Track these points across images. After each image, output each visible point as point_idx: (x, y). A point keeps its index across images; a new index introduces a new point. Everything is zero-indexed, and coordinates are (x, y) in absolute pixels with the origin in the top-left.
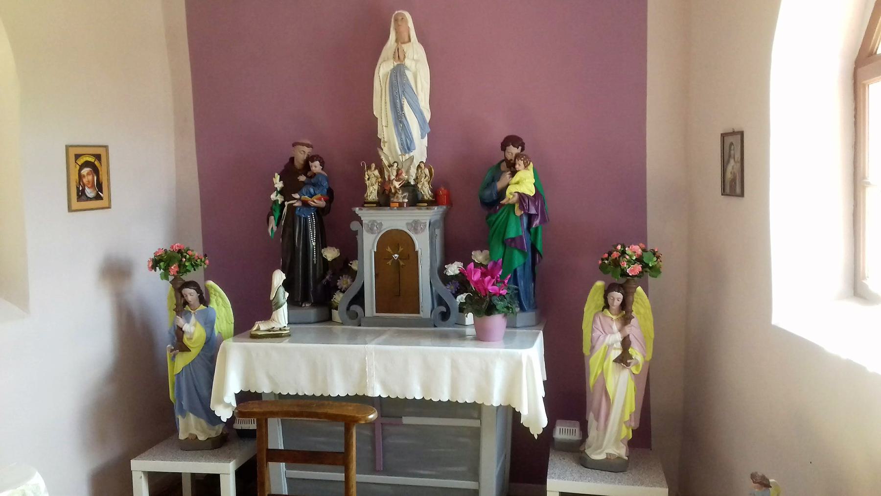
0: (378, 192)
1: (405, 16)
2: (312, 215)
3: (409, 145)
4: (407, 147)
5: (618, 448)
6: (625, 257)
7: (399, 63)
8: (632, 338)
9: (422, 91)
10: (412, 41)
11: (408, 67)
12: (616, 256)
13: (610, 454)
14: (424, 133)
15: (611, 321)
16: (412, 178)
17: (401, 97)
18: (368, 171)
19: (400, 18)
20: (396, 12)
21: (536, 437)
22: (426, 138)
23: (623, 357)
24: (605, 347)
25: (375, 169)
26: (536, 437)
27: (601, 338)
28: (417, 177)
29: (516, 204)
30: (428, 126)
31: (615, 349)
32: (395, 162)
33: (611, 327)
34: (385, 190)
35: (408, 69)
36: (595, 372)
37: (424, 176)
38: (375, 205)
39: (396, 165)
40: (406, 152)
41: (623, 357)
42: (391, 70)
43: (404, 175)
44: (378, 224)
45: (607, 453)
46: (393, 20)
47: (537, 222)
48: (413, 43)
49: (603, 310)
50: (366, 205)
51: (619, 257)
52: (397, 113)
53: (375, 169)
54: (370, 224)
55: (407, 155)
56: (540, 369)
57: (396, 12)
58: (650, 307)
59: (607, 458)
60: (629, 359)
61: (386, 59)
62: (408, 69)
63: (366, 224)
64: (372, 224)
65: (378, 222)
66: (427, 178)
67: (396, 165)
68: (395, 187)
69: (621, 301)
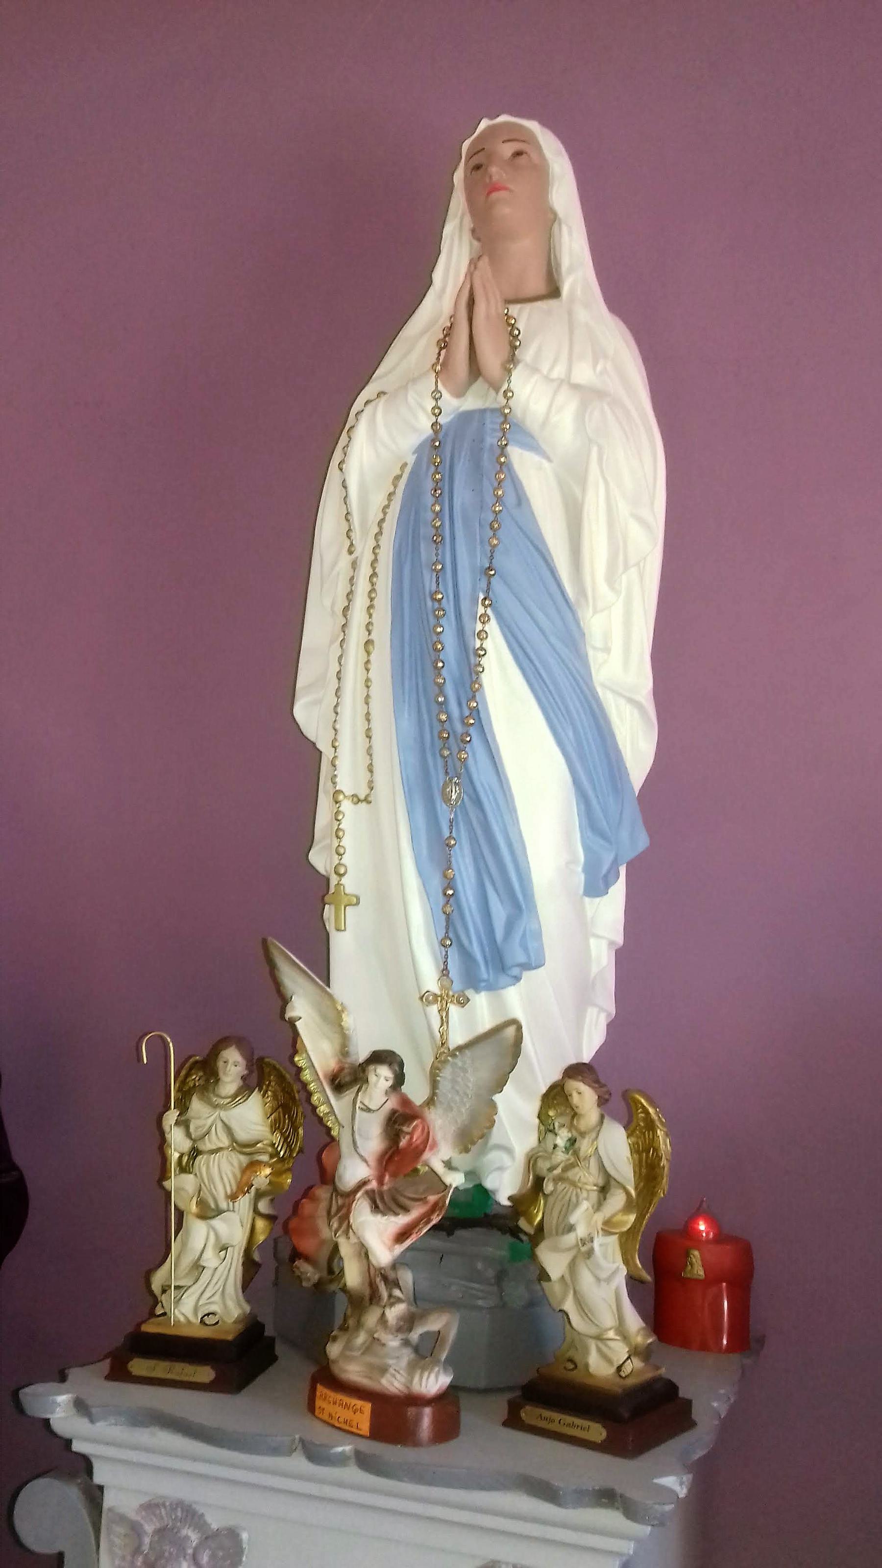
0: (250, 1266)
1: (529, 139)
3: (499, 934)
4: (277, 1134)
7: (471, 402)
9: (611, 580)
10: (565, 290)
11: (533, 424)
14: (607, 859)
16: (505, 1158)
17: (465, 605)
18: (196, 1105)
19: (507, 150)
20: (484, 124)
22: (618, 890)
25: (246, 1088)
28: (539, 1182)
30: (632, 812)
32: (378, 1057)
34: (296, 1255)
35: (531, 444)
37: (589, 1177)
38: (205, 1374)
39: (382, 1076)
40: (473, 982)
42: (419, 450)
43: (435, 1160)
44: (209, 1537)
46: (459, 176)
48: (572, 299)
50: (139, 1366)
53: (246, 1088)
54: (149, 1528)
55: (480, 1000)
56: (524, 835)
57: (484, 124)
61: (607, 1097)
62: (531, 444)
63: (122, 1519)
64: (161, 1532)
65: (215, 1522)
66: (617, 1200)
67: (382, 1076)
68: (364, 1253)
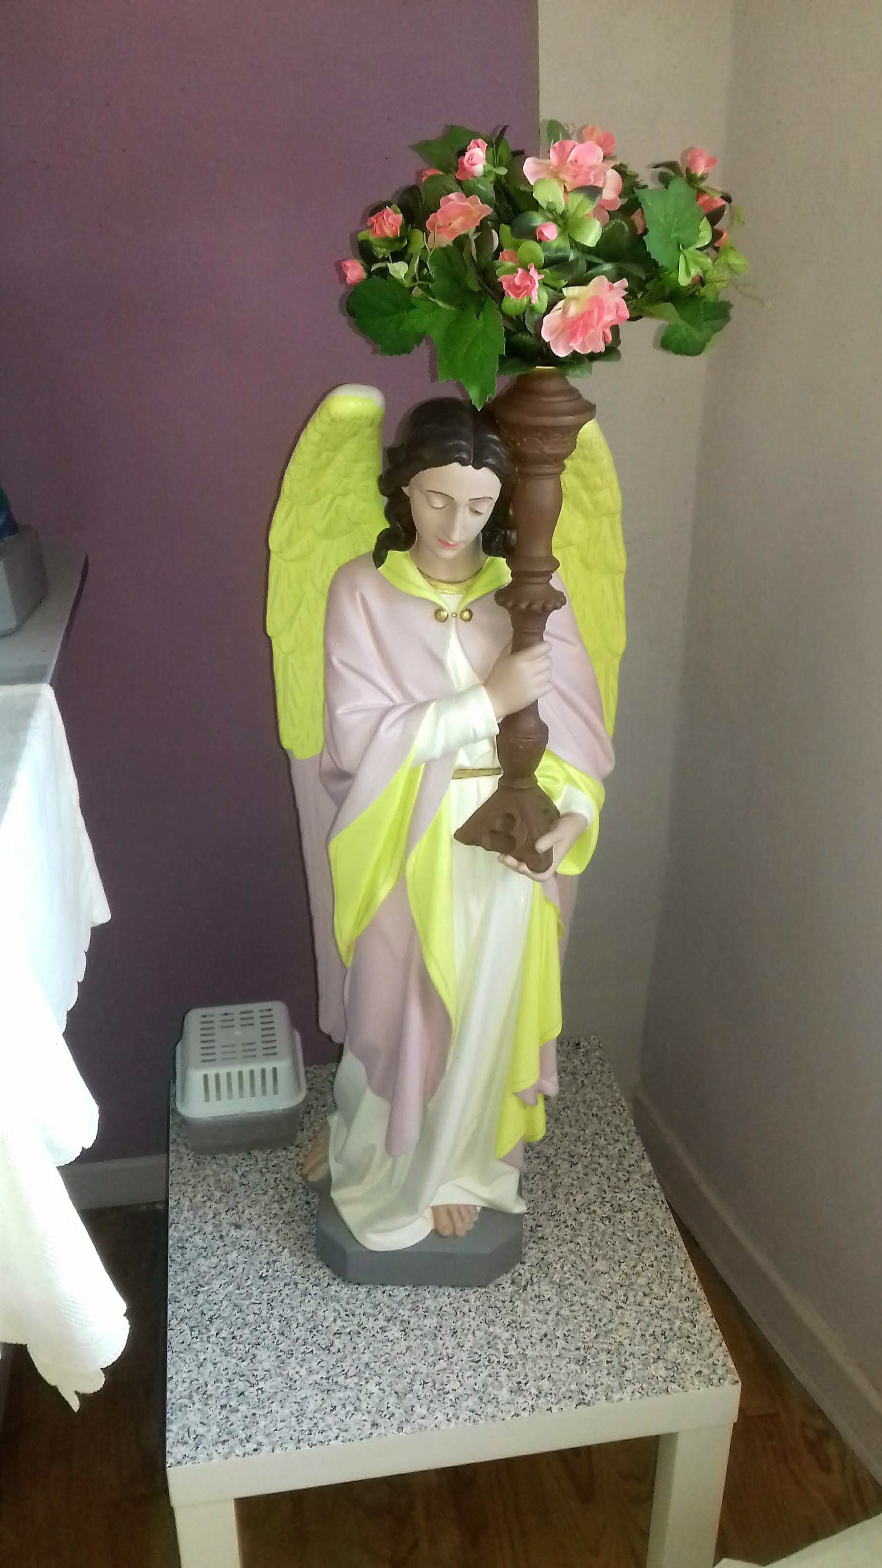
2: (495, 538)
5: (486, 1178)
6: (533, 234)
8: (548, 712)
12: (457, 224)
13: (449, 1210)
15: (434, 624)
21: (75, 1404)
23: (510, 818)
24: (414, 770)
26: (75, 1404)
27: (389, 733)
29: (525, 1308)
31: (462, 773)
33: (439, 663)
36: (363, 890)
41: (510, 818)
45: (435, 1210)
47: (172, 1081)
49: (379, 558)
51: (482, 228)
52: (328, 704)
58: (621, 562)
59: (436, 1233)
60: (542, 834)
69: (487, 510)
